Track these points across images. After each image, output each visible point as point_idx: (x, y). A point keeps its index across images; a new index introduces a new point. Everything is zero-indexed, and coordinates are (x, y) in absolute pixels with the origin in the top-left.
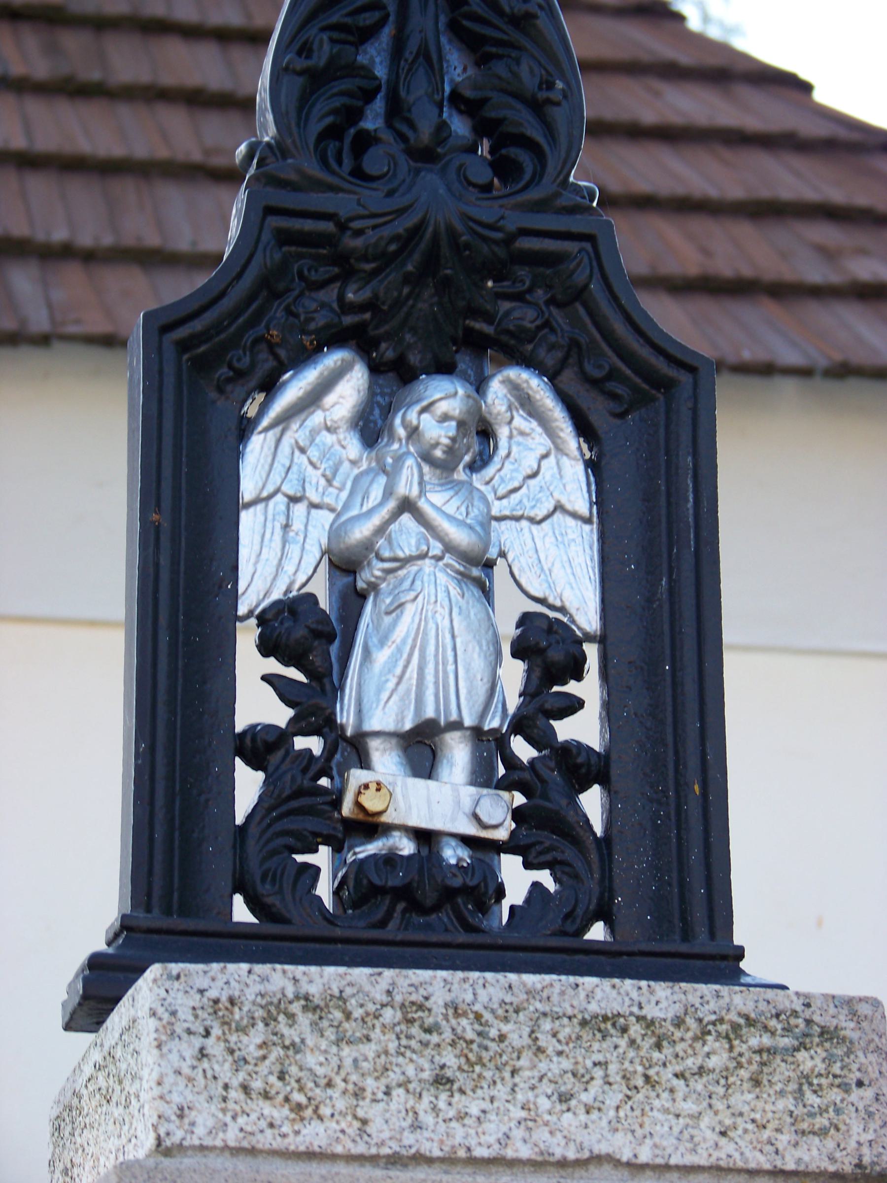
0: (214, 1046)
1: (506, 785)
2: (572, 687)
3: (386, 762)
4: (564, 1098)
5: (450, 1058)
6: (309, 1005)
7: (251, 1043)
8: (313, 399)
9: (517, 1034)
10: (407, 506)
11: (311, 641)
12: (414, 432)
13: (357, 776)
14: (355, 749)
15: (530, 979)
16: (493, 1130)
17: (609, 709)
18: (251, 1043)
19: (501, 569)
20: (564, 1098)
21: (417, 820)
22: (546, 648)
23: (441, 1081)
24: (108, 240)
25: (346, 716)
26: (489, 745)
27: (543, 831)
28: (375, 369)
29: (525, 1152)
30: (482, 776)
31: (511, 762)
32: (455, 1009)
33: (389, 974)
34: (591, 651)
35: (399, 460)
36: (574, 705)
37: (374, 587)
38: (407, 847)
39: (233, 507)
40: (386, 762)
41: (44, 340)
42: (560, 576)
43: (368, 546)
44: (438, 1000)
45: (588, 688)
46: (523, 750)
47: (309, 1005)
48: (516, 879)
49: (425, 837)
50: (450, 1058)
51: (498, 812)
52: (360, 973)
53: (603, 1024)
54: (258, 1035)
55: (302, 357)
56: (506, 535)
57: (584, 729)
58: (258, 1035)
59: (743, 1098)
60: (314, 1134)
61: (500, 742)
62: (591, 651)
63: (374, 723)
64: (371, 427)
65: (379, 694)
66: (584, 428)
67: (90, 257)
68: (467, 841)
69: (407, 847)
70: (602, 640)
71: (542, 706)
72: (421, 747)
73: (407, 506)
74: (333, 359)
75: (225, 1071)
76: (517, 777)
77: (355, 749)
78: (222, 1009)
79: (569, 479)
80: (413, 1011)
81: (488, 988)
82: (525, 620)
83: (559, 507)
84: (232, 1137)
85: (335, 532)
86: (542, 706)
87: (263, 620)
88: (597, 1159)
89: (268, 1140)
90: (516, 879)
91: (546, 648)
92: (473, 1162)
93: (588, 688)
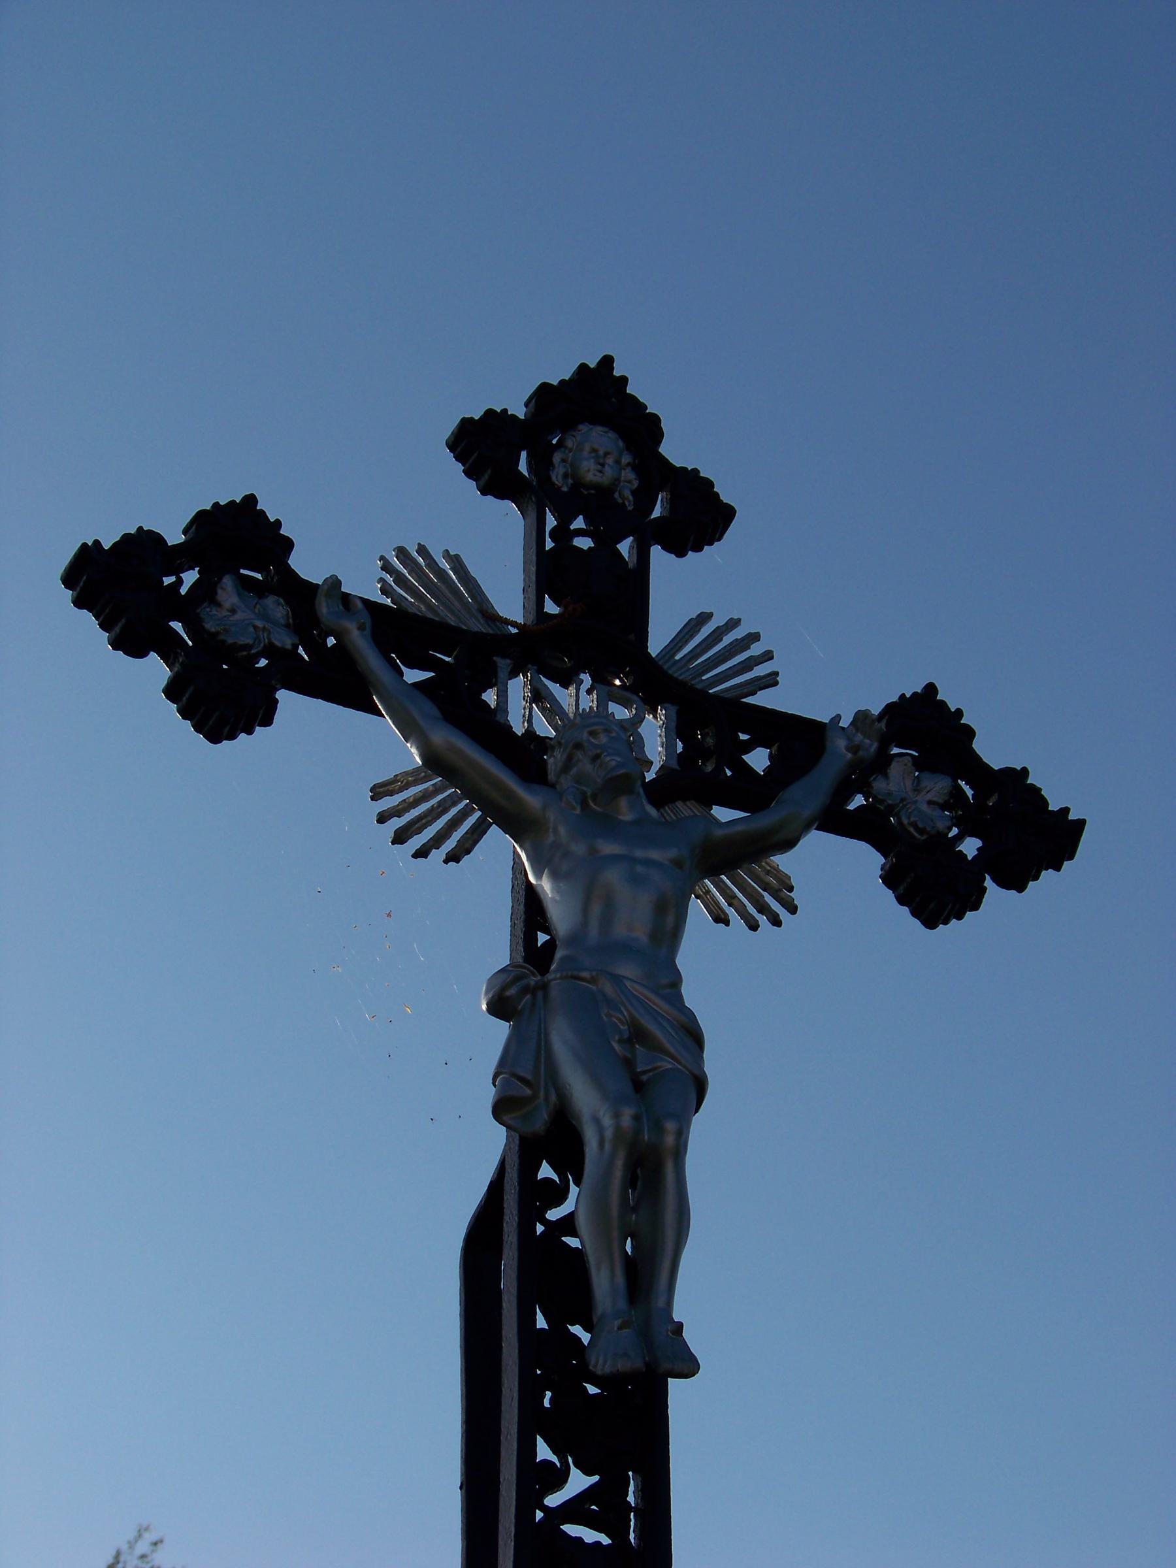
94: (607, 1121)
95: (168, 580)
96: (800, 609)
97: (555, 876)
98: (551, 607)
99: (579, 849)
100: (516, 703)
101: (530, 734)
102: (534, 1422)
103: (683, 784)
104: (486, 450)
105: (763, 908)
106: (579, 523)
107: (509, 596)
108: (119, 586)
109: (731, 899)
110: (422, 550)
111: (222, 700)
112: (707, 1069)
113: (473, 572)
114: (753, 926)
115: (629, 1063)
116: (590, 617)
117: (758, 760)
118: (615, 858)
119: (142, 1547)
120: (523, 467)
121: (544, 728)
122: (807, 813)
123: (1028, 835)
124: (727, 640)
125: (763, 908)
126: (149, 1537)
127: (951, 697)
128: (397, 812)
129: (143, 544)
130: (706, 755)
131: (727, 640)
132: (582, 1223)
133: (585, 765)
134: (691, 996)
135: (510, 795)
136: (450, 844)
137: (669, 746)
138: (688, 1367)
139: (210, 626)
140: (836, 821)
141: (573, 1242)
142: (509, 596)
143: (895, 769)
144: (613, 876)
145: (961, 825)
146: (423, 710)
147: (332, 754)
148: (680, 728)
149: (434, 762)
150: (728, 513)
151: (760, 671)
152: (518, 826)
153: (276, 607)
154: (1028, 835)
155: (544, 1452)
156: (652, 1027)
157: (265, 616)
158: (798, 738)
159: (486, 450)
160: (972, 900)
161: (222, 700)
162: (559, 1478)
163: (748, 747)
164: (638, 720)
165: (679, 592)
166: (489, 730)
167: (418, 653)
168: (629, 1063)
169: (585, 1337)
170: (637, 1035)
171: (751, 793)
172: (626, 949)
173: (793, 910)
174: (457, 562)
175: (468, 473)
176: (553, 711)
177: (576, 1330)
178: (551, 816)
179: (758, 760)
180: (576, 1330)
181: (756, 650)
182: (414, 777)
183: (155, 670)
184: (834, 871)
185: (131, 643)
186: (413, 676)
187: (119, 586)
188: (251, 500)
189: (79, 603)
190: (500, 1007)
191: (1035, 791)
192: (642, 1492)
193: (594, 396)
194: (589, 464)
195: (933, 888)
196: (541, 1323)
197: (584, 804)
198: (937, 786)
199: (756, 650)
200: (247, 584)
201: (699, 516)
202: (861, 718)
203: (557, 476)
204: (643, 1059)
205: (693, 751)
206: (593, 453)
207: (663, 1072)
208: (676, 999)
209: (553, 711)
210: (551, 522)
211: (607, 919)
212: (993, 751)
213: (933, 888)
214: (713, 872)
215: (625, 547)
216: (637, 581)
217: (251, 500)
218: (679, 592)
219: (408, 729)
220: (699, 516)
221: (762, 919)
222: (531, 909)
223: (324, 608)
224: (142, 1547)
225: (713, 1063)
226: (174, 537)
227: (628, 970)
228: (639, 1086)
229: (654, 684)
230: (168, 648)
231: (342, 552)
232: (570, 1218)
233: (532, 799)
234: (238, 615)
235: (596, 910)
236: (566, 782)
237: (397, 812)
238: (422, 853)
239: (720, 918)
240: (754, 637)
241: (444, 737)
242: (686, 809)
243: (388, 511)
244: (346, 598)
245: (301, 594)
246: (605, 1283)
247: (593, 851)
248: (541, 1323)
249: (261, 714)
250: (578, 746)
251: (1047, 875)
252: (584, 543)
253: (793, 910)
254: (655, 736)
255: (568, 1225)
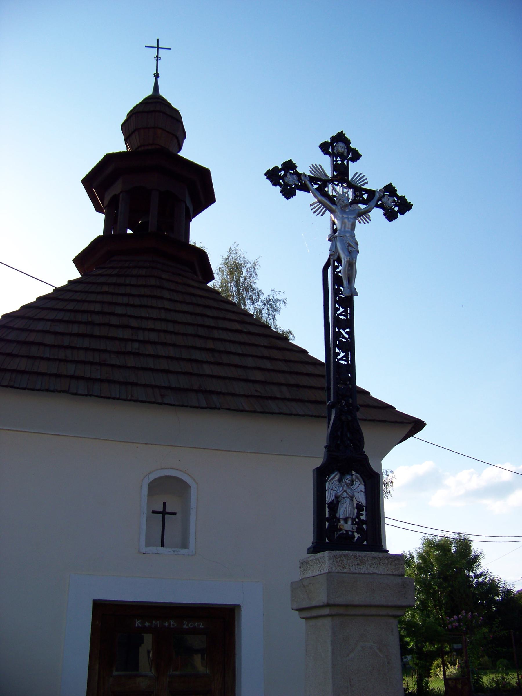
0: (334, 560)
1: (355, 524)
2: (362, 513)
3: (342, 522)
4: (371, 566)
5: (359, 562)
6: (344, 556)
7: (338, 560)
8: (334, 477)
9: (366, 559)
10: (345, 491)
11: (334, 506)
12: (345, 482)
13: (339, 524)
14: (339, 520)
15: (367, 553)
16: (364, 570)
17: (366, 515)
18: (338, 560)
19: (354, 498)
20: (371, 566)
21: (346, 529)
22: (359, 507)
23: (358, 564)
24: (226, 392)
25: (338, 516)
26: (353, 519)
27: (359, 530)
28: (340, 473)
29: (367, 572)
30: (352, 524)
31: (356, 521)
32: (359, 556)
33: (352, 552)
34: (364, 508)
35: (344, 485)
36: (362, 515)
37: (341, 500)
38: (345, 532)
39: (325, 490)
40: (342, 522)
41: (219, 409)
42: (361, 499)
43: (340, 496)
44: (358, 555)
45: (364, 512)
46: (357, 520)
47: (344, 556)
48: (356, 535)
49: (347, 531)
50: (359, 562)
51: (355, 527)
52: (350, 552)
53: (374, 558)
54: (339, 559)
55: (332, 473)
56: (356, 494)
57: (363, 518)
58: (339, 559)
59: (389, 566)
60: (345, 570)
61: (355, 519)
62: (364, 508)
63: (341, 517)
64: (340, 481)
65: (341, 513)
66: (364, 481)
67: (224, 394)
68: (351, 531)
69: (345, 532)
70: (366, 507)
71: (359, 515)
72: (346, 520)
73: (345, 491)
74: (336, 473)
75: (335, 563)
76: (357, 523)
77: (339, 520)
78: (335, 556)
79: (362, 488)
80: (355, 556)
81: (363, 553)
82: (357, 504)
83: (361, 491)
84: (336, 571)
85: (336, 494)
86: (359, 515)
87: (328, 504)
88: (374, 573)
89: (340, 571)
90: (356, 535)
91: (359, 507)
92: (362, 574)
93: (364, 512)
94: (345, 258)
95: (280, 173)
96: (371, 172)
97: (337, 219)
98: (335, 173)
99: (340, 216)
100: (330, 189)
101: (332, 195)
102: (335, 302)
103: (355, 202)
104: (324, 147)
105: (366, 221)
106: (338, 159)
107: (329, 172)
108: (272, 175)
109: (362, 219)
110: (315, 165)
111: (288, 193)
112: (359, 249)
113: (323, 168)
114: (365, 223)
115: (348, 249)
116: (341, 174)
117: (365, 196)
118: (346, 218)
119: (235, 246)
120: (330, 150)
121: (335, 194)
122: (373, 206)
123: (405, 206)
124: (361, 176)
125: (366, 221)
126: (236, 244)
127: (393, 185)
128: (314, 208)
129: (276, 169)
130: (358, 196)
131: (361, 176)
132: (342, 272)
133: (341, 202)
134: (357, 238)
135: (330, 207)
136: (321, 213)
137: (353, 195)
138: (356, 294)
139: (286, 181)
140: (377, 206)
141: (340, 274)
142: (329, 172)
143: (385, 197)
144: (346, 220)
145: (394, 205)
146: (317, 194)
147: (304, 199)
148: (354, 192)
149: (319, 201)
150: (361, 156)
151: (365, 181)
152: (332, 211)
153: (295, 177)
154: (405, 206)
155: (337, 306)
156: (351, 243)
157: (294, 179)
158: (371, 193)
159: (324, 147)
160: (396, 217)
161: (288, 193)
162: (339, 309)
163: (364, 194)
164: (348, 191)
165: (354, 168)
166: (326, 195)
167: (317, 183)
168: (348, 249)
169: (342, 289)
170: (349, 245)
171: (364, 202)
172: (348, 232)
173: (370, 220)
174: (320, 166)
175: (322, 151)
176: (336, 191)
177: (341, 288)
178: (337, 210)
179: (365, 196)
180: (341, 288)
181: (365, 178)
182: (315, 203)
183: (278, 188)
184: (377, 214)
185: (275, 185)
186: (316, 186)
187: (272, 175)
188: (291, 160)
189: (267, 178)
190: (330, 240)
191: (406, 199)
192: (350, 311)
193: (340, 138)
194: (340, 148)
195: (391, 216)
196: (336, 287)
197: (341, 208)
198: (391, 199)
199: (365, 178)
200: (291, 173)
201: (356, 156)
202: (380, 190)
203: (335, 151)
204: (350, 249)
205: (356, 196)
206: (340, 147)
207: (353, 250)
208: (355, 239)
209: (336, 191)
210: (335, 159)
211: (345, 228)
212: (399, 193)
213: (391, 216)
214: (360, 217)
215: (345, 162)
216: (347, 168)
217: (291, 160)
218: (354, 168)
219: (315, 197)
220: (356, 156)
221: (366, 222)
222: (334, 223)
223: (303, 178)
224: (235, 246)
225: (360, 249)
226: (280, 167)
227: (348, 235)
228: (349, 252)
229: (350, 185)
230: (280, 185)
231: (304, 168)
232: (340, 271)
233: (334, 207)
234: (291, 179)
235: (343, 226)
236: (338, 205)
237: (314, 208)
238: (317, 215)
239: (360, 223)
240: (364, 176)
241: (321, 198)
242: (355, 205)
243: (311, 160)
244: (305, 175)
245: (299, 175)
246: (345, 282)
247: (343, 216)
248: (336, 287)
249: (294, 194)
250: (340, 199)
251: (407, 212)
252: (339, 162)
253: (370, 220)
254: (350, 194)
255: (340, 272)
